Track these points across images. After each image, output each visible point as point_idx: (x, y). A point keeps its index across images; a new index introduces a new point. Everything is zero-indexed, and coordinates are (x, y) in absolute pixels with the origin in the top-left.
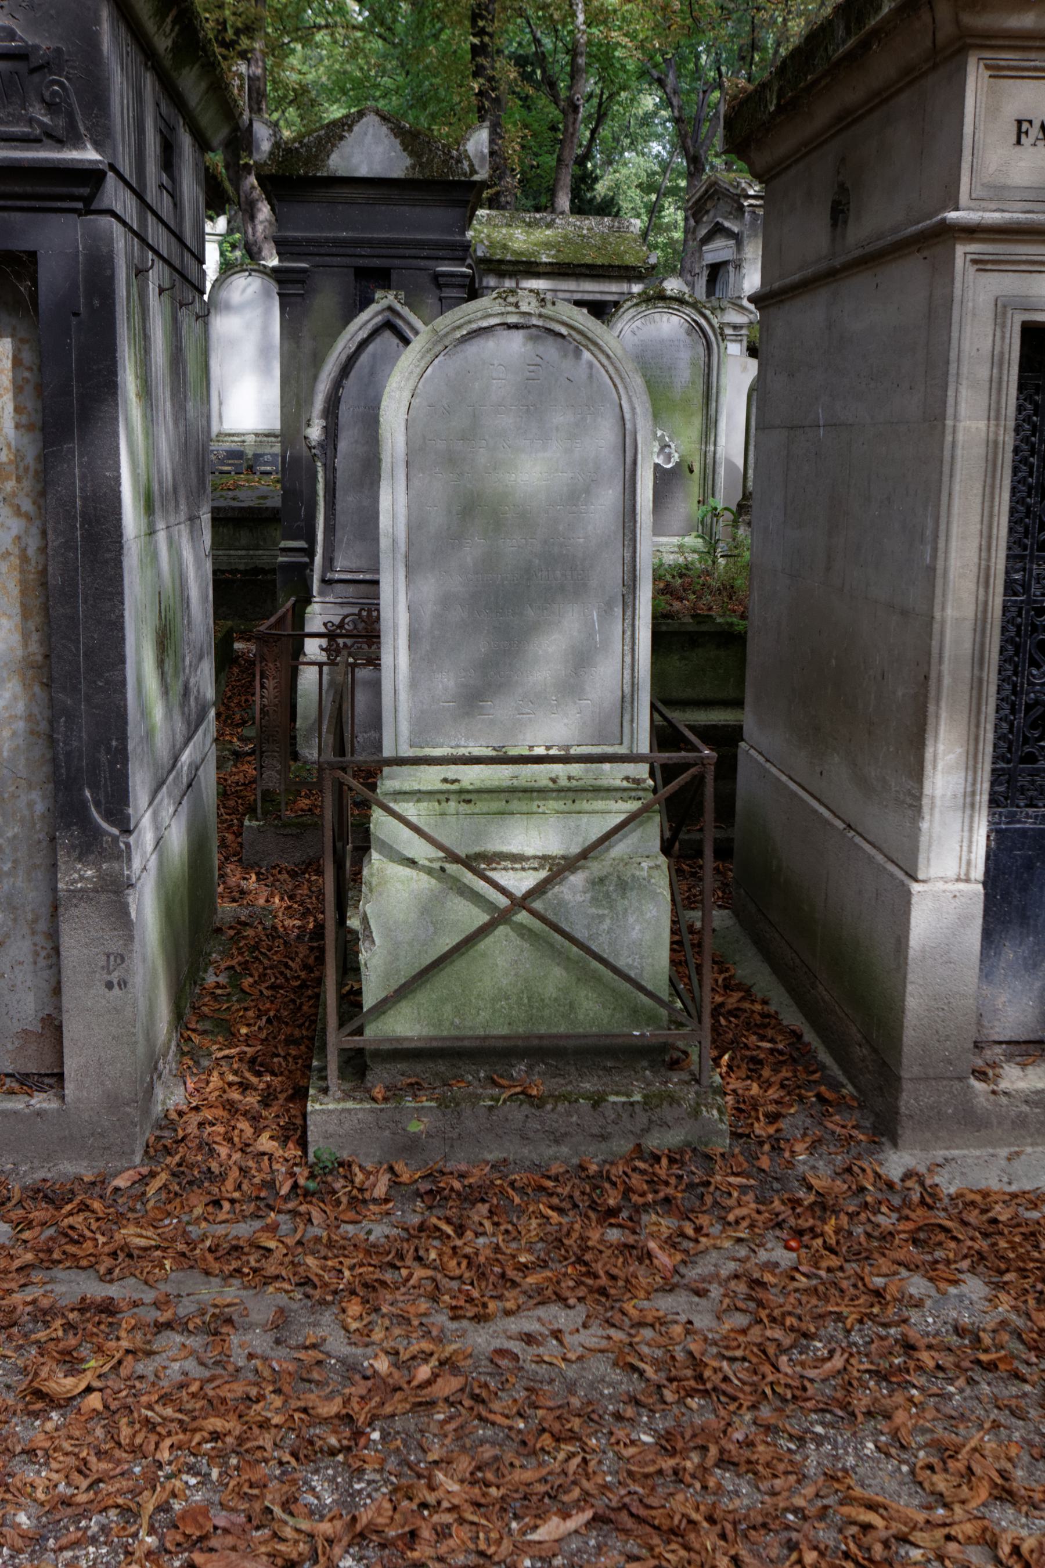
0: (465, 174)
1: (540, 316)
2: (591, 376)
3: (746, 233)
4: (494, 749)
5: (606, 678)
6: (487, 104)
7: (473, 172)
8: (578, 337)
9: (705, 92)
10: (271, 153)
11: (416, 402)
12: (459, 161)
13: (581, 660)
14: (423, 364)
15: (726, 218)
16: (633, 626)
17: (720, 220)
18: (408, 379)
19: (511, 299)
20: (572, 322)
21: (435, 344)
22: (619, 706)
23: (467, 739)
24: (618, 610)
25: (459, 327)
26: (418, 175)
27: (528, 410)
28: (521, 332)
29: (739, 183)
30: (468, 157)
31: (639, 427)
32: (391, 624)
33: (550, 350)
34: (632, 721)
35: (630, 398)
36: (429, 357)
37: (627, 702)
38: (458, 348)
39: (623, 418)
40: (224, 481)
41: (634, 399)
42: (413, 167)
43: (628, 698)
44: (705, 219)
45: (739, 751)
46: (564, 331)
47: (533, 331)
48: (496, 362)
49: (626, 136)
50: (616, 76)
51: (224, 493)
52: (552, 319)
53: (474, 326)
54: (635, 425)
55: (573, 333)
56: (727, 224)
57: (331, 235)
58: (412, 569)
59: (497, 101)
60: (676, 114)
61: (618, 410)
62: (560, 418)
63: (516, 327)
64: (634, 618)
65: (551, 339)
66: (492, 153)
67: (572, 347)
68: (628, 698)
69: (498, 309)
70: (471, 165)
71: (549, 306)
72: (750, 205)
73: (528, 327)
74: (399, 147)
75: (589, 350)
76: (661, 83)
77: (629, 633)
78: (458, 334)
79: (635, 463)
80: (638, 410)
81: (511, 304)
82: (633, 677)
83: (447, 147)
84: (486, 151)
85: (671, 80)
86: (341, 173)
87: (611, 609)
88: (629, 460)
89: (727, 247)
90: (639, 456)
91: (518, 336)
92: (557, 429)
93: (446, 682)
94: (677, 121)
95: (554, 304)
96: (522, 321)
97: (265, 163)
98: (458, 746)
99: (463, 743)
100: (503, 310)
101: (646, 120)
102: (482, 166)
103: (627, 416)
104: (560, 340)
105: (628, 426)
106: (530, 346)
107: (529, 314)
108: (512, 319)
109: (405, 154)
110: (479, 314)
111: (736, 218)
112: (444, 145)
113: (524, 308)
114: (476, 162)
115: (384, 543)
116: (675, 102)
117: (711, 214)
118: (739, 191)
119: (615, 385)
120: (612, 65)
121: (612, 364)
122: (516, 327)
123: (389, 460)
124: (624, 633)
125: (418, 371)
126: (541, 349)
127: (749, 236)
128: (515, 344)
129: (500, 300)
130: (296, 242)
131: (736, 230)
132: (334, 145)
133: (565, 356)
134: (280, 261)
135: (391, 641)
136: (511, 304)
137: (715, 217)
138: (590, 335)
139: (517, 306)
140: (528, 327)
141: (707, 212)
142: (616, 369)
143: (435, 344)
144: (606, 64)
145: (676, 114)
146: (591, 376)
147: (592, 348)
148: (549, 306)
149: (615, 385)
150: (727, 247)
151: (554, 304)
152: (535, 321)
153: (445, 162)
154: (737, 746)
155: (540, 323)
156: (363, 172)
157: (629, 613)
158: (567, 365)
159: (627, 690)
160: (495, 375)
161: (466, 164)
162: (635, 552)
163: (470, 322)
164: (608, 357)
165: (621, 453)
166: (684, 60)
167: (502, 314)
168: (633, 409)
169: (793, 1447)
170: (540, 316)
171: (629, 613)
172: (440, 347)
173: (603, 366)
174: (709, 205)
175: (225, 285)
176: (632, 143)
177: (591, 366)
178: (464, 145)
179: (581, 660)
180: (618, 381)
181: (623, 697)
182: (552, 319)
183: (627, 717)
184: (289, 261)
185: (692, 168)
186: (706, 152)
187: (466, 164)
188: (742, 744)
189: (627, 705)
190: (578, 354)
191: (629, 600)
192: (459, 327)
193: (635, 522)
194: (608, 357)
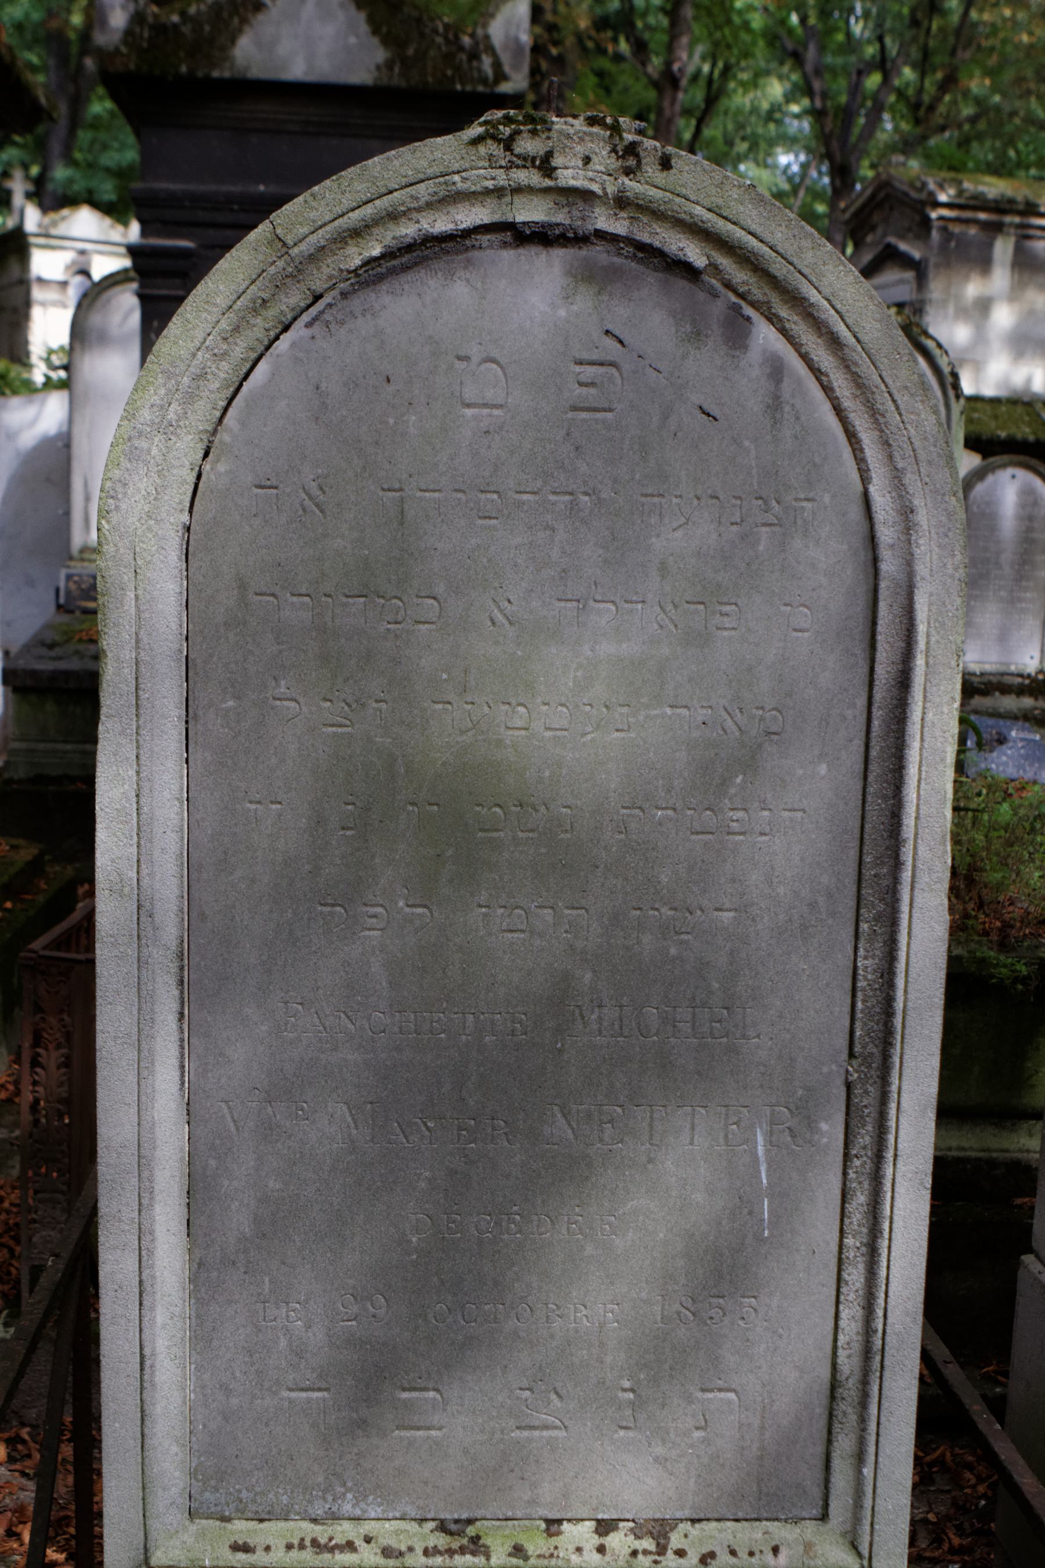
0: (484, 81)
1: (621, 202)
2: (775, 406)
3: (933, 260)
4: (443, 1527)
5: (786, 1341)
6: (544, 65)
7: (501, 76)
8: (740, 276)
9: (860, 73)
10: (128, 33)
11: (217, 470)
12: (474, 56)
13: (722, 1271)
14: (240, 350)
15: (902, 237)
16: (876, 1178)
17: (892, 240)
18: (190, 398)
19: (527, 145)
20: (722, 226)
21: (279, 286)
22: (820, 1410)
23: (361, 1497)
24: (831, 1130)
25: (356, 233)
26: (397, 80)
27: (573, 507)
28: (559, 254)
29: (924, 185)
30: (491, 49)
31: (921, 569)
32: (130, 1160)
33: (649, 317)
34: (860, 1457)
35: (897, 477)
36: (259, 328)
37: (844, 1398)
38: (356, 303)
39: (872, 540)
40: (85, 626)
41: (909, 478)
42: (389, 65)
43: (850, 1389)
44: (869, 239)
45: (1021, 1273)
46: (695, 254)
47: (598, 253)
48: (475, 352)
49: (743, 139)
50: (736, 37)
51: (81, 647)
52: (657, 214)
53: (408, 230)
54: (909, 564)
55: (725, 262)
56: (903, 246)
57: (236, 188)
58: (203, 984)
59: (559, 62)
60: (818, 104)
61: (855, 512)
62: (682, 536)
63: (542, 237)
64: (879, 1158)
65: (652, 279)
66: (537, 49)
67: (717, 309)
68: (850, 1389)
69: (484, 177)
70: (497, 65)
71: (651, 169)
72: (941, 218)
73: (580, 240)
74: (364, 28)
75: (772, 318)
76: (797, 58)
77: (860, 1199)
78: (354, 257)
79: (904, 682)
80: (922, 517)
81: (527, 161)
82: (868, 1330)
83: (453, 31)
84: (525, 38)
85: (811, 54)
86: (256, 72)
87: (811, 1124)
88: (884, 671)
89: (901, 282)
90: (920, 661)
91: (549, 267)
92: (663, 569)
93: (307, 1316)
94: (817, 115)
95: (666, 164)
96: (561, 217)
97: (117, 50)
98: (335, 1517)
99: (347, 1508)
100: (502, 178)
101: (773, 115)
102: (516, 67)
103: (886, 535)
104: (681, 284)
105: (889, 565)
106: (584, 302)
107: (586, 195)
108: (530, 212)
109: (375, 41)
110: (423, 191)
111: (918, 237)
112: (447, 26)
113: (570, 176)
114: (505, 59)
115: (110, 913)
116: (817, 85)
117: (880, 231)
118: (923, 196)
119: (851, 435)
120: (729, 21)
121: (846, 365)
122: (542, 237)
123: (128, 654)
124: (845, 1196)
125: (225, 371)
126: (620, 313)
127: (937, 266)
128: (534, 300)
129: (491, 147)
130: (172, 201)
131: (917, 255)
132: (244, 21)
133: (697, 336)
134: (144, 233)
135: (130, 1213)
136: (527, 161)
137: (885, 235)
138: (779, 268)
139: (545, 165)
140: (580, 240)
141: (873, 228)
142: (858, 382)
143: (279, 286)
144: (721, 19)
145: (818, 104)
146: (775, 406)
147: (784, 312)
148: (651, 169)
149: (851, 435)
150: (901, 282)
151: (666, 164)
152: (603, 220)
153: (449, 58)
154: (1017, 1264)
155: (620, 227)
156: (297, 71)
157: (864, 1138)
158: (704, 363)
159: (849, 1363)
160: (470, 393)
161: (487, 62)
162: (891, 957)
163: (393, 216)
164: (834, 342)
165: (860, 650)
166: (831, 31)
167: (498, 192)
168: (906, 512)
169: (780, 1330)
170: (621, 202)
171: (864, 1138)
172: (295, 298)
173: (817, 372)
174: (876, 218)
175: (99, 303)
176: (750, 149)
177: (776, 370)
178: (485, 26)
179: (722, 1271)
180: (861, 423)
181: (834, 1385)
182: (657, 214)
183: (844, 1444)
184: (158, 234)
185: (838, 182)
186: (859, 159)
187: (487, 62)
188: (1028, 1259)
189: (847, 1409)
190: (736, 331)
191: (867, 1101)
192: (356, 233)
193: (897, 865)
194: (834, 342)
